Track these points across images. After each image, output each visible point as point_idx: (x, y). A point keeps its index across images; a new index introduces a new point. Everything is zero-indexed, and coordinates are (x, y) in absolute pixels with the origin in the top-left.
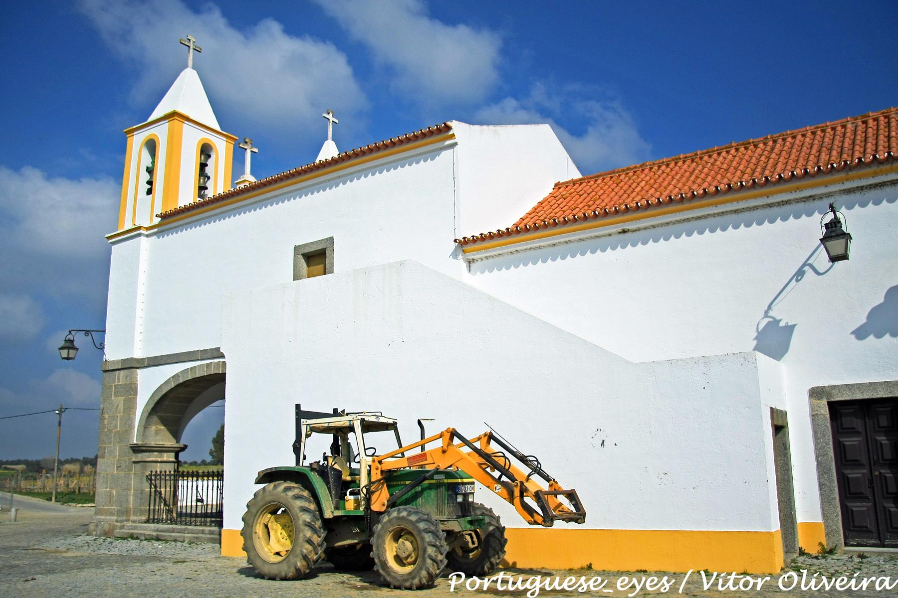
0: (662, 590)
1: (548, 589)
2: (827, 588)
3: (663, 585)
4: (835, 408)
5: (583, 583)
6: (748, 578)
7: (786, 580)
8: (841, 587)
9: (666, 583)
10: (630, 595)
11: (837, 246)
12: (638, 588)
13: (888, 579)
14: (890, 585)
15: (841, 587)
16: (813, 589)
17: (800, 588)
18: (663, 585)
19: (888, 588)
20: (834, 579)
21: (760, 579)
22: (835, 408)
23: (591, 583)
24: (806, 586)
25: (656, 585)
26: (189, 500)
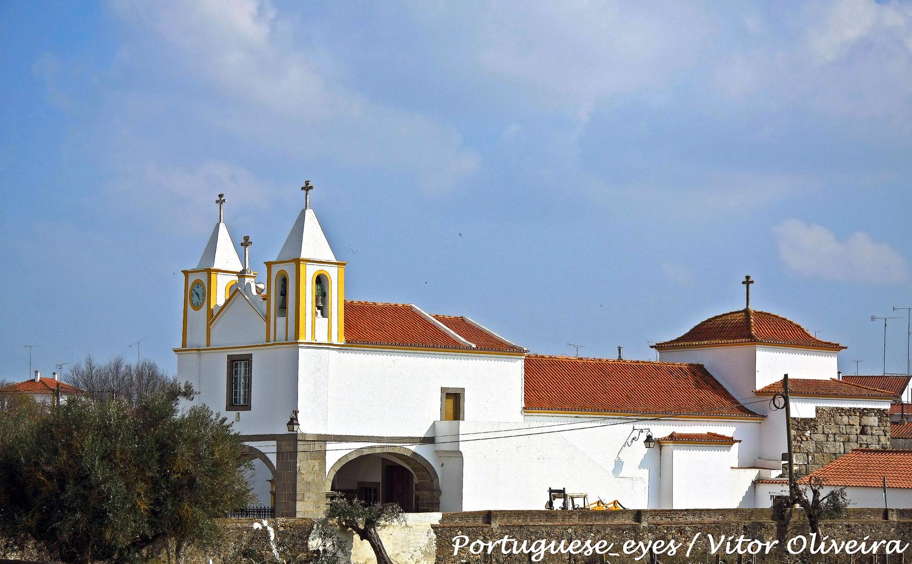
0: (585, 553)
1: (553, 552)
3: (670, 548)
5: (673, 547)
9: (673, 547)
18: (670, 548)
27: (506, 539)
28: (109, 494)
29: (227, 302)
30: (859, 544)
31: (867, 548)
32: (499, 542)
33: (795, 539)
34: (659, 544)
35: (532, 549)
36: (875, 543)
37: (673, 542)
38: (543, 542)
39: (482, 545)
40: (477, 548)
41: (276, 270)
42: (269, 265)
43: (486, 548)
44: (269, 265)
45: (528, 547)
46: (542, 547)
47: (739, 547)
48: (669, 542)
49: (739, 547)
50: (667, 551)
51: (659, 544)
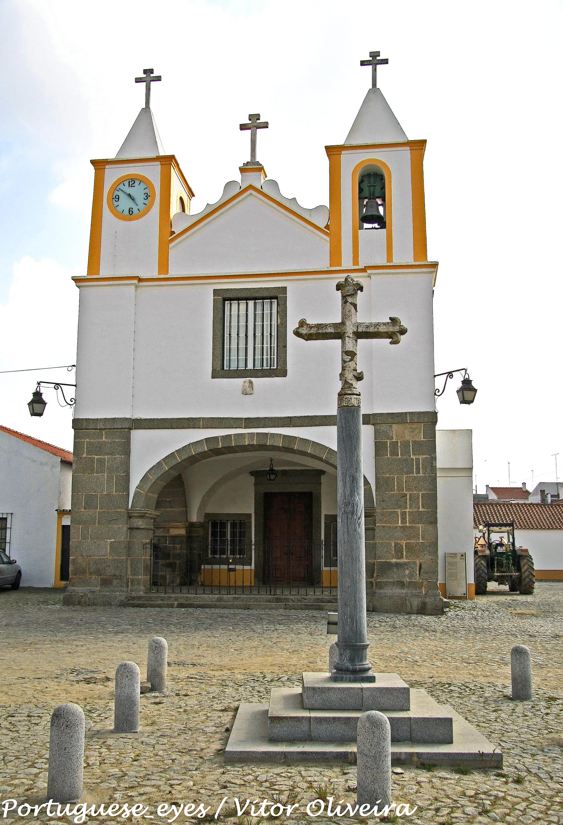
0: (199, 816)
1: (93, 815)
2: (352, 814)
3: (200, 811)
4: (312, 579)
5: (202, 810)
6: (279, 805)
7: (313, 806)
8: (189, 813)
9: (202, 810)
10: (169, 821)
11: (37, 406)
12: (177, 814)
13: (407, 806)
14: (341, 813)
15: (189, 813)
16: (339, 814)
17: (46, 812)
18: (200, 811)
19: (408, 814)
20: (357, 806)
21: (37, 806)
22: (312, 579)
23: (134, 809)
24: (61, 812)
25: (117, 812)
26: (259, 312)
27: (51, 802)
28: (207, 684)
29: (212, 212)
30: (372, 808)
31: (379, 810)
32: (44, 805)
33: (314, 803)
34: (366, 807)
35: (75, 812)
36: (387, 806)
37: (202, 805)
38: (85, 805)
39: (29, 808)
40: (24, 810)
41: (351, 164)
42: (99, 165)
43: (32, 811)
44: (99, 165)
45: (71, 810)
46: (84, 810)
47: (262, 810)
48: (199, 805)
49: (262, 810)
50: (122, 813)
51: (366, 807)
